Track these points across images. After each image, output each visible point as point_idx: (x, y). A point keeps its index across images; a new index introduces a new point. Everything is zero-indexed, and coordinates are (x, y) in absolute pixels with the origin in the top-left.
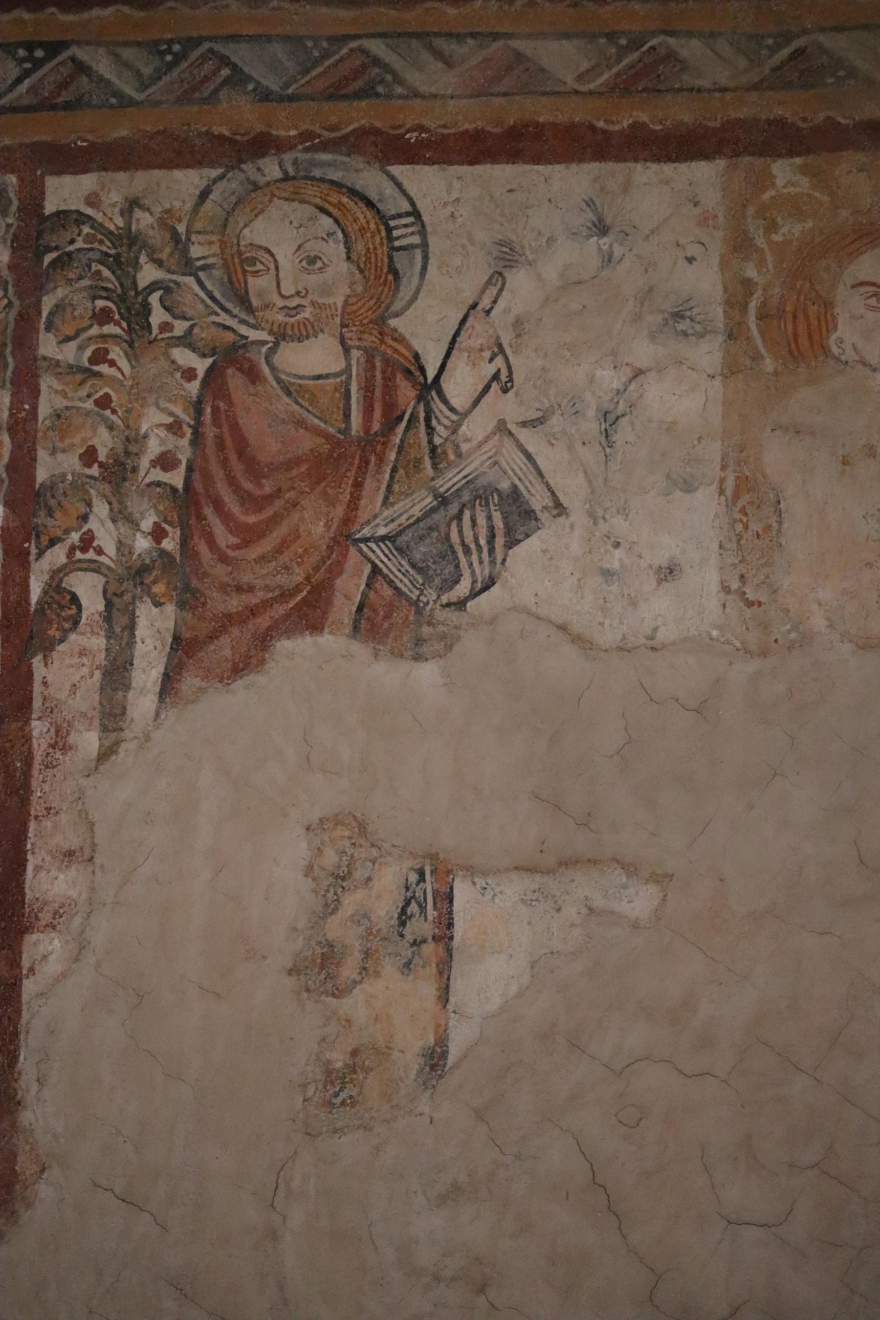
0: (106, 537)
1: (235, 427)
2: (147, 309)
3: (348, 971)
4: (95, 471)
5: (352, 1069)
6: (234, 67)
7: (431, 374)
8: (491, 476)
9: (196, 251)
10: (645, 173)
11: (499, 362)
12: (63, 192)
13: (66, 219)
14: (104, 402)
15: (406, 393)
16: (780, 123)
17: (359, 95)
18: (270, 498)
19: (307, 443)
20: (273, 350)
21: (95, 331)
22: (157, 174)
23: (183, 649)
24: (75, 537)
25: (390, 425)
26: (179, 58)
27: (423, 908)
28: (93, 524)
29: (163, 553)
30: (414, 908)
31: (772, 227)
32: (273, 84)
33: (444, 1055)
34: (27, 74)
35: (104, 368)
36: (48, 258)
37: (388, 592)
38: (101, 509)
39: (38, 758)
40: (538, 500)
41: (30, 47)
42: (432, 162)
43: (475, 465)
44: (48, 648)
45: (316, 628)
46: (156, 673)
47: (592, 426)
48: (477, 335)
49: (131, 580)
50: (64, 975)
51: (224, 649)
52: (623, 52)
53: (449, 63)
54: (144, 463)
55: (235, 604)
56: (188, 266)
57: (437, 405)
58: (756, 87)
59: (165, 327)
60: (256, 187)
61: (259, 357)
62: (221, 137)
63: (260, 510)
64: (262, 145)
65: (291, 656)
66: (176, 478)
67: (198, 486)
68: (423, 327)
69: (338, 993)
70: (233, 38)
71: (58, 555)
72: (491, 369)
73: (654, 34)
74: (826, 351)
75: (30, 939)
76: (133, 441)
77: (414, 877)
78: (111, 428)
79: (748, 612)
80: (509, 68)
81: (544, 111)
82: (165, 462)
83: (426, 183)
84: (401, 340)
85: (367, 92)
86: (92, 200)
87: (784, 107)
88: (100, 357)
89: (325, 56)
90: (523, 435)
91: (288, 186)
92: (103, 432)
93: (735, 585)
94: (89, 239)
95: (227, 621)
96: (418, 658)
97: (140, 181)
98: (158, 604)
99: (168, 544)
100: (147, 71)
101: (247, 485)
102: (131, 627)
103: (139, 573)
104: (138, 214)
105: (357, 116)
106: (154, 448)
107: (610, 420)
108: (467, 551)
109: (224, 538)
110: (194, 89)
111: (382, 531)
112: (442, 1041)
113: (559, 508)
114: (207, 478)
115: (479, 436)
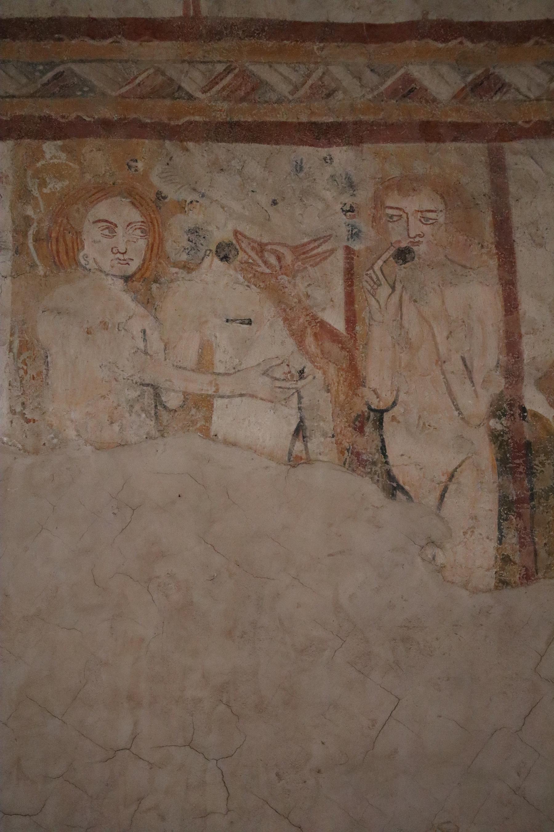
31: (43, 184)
58: (32, 96)
87: (52, 109)
93: (19, 409)
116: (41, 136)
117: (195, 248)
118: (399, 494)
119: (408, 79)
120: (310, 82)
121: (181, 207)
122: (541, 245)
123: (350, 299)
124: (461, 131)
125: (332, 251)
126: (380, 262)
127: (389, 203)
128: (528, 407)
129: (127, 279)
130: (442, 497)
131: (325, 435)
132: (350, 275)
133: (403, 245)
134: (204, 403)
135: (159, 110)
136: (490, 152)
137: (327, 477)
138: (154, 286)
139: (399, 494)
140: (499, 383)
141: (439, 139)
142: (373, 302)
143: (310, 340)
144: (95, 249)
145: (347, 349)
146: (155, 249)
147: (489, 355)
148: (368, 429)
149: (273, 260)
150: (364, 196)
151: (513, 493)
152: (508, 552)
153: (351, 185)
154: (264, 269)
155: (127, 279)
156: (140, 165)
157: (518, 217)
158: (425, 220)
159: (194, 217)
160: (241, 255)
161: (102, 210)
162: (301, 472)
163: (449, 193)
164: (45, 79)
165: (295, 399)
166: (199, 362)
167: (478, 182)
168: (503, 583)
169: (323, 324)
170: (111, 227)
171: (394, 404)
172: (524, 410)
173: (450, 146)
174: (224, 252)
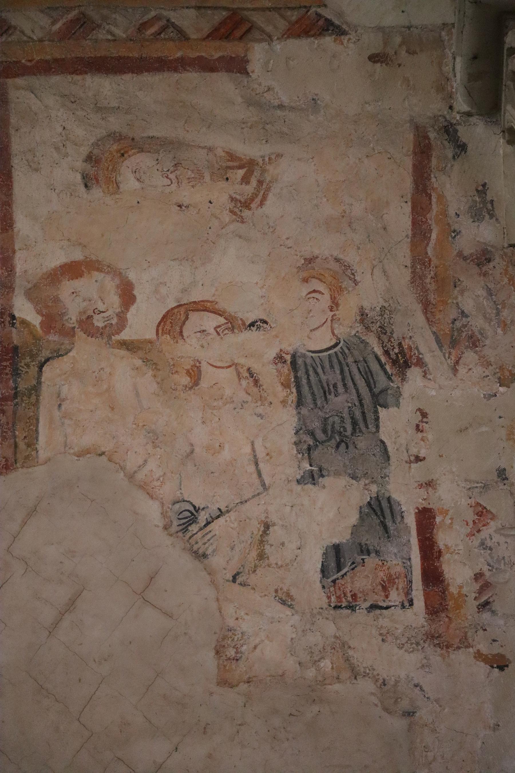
172: (13, 317)
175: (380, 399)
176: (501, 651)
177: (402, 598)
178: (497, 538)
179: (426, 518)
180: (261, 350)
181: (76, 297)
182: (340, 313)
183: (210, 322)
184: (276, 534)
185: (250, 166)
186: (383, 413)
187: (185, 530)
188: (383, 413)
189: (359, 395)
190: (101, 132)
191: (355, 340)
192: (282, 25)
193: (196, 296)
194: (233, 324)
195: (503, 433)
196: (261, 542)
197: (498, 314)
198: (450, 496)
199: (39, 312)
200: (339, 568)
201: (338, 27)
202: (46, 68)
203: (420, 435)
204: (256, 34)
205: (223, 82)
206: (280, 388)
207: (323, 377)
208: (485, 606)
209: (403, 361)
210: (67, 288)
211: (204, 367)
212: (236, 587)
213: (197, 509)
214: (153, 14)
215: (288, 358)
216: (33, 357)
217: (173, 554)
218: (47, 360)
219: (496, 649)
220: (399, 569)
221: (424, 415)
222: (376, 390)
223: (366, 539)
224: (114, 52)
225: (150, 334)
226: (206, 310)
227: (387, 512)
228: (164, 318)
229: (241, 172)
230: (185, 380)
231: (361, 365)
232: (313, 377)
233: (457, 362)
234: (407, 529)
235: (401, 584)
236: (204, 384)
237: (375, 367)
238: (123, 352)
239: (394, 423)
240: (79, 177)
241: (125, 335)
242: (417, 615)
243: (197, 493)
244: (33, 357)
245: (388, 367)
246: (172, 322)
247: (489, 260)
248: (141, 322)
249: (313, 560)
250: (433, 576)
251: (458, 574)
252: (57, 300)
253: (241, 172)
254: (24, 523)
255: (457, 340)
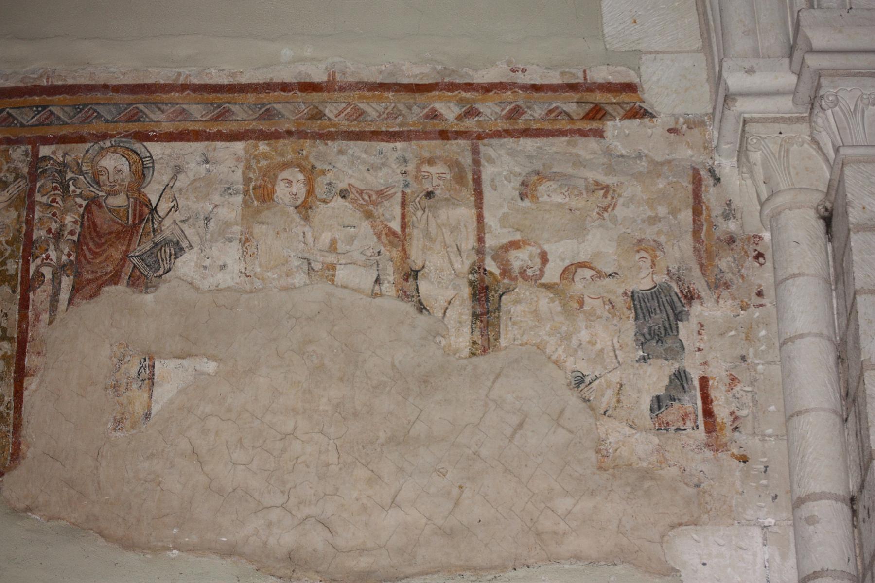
0: (53, 255)
1: (94, 222)
2: (68, 186)
3: (122, 389)
4: (51, 235)
5: (122, 419)
6: (98, 113)
7: (154, 205)
8: (171, 237)
9: (84, 168)
10: (219, 144)
11: (175, 202)
12: (45, 151)
13: (45, 158)
14: (54, 215)
15: (146, 210)
16: (261, 130)
17: (135, 121)
18: (103, 244)
19: (116, 227)
20: (106, 199)
21: (52, 193)
22: (74, 145)
23: (76, 289)
24: (44, 255)
25: (140, 222)
26: (81, 110)
27: (145, 370)
28: (50, 252)
29: (71, 261)
30: (142, 370)
31: (258, 162)
32: (109, 118)
33: (150, 414)
34: (36, 115)
35: (55, 204)
36: (40, 171)
37: (138, 273)
38: (52, 247)
39: (30, 323)
40: (184, 244)
41: (37, 107)
42: (157, 141)
43: (167, 233)
44: (34, 290)
45: (116, 284)
46: (67, 297)
47: (202, 223)
48: (168, 194)
49: (60, 269)
50: (36, 390)
51: (88, 290)
52: (215, 109)
53: (163, 112)
54: (66, 233)
55: (90, 277)
56: (81, 173)
57: (156, 216)
58: (254, 120)
59: (74, 191)
60: (102, 148)
61: (101, 200)
62: (93, 134)
63: (101, 247)
64: (105, 136)
65: (108, 292)
66: (75, 238)
67: (81, 240)
68: (152, 193)
69: (118, 396)
70: (99, 104)
71: (38, 261)
72: (172, 204)
73: (225, 103)
74: (273, 200)
75: (26, 379)
76: (63, 226)
77: (143, 360)
78: (56, 222)
79: (247, 279)
80: (181, 113)
81: (191, 127)
82: (72, 233)
83: (156, 149)
84: (145, 195)
85: (138, 120)
86: (54, 153)
87: (264, 126)
88: (54, 201)
89: (126, 109)
90: (180, 224)
91: (112, 149)
92: (54, 223)
93: (243, 271)
94: (52, 165)
95: (89, 282)
96: (147, 293)
97: (68, 147)
98: (68, 276)
99: (72, 258)
100: (72, 114)
101: (97, 240)
102: (60, 283)
103: (63, 266)
104: (67, 157)
105: (134, 127)
106: (69, 228)
107: (207, 219)
108: (163, 261)
109: (89, 256)
110: (86, 120)
111: (137, 254)
112: (149, 407)
113: (191, 247)
114: (85, 237)
115: (168, 229)
116: (258, 139)
117: (330, 192)
118: (424, 311)
119: (434, 110)
120: (387, 112)
121: (323, 172)
122: (495, 190)
123: (403, 216)
124: (459, 134)
125: (395, 193)
126: (418, 199)
127: (423, 170)
128: (487, 268)
129: (296, 208)
130: (445, 312)
131: (389, 282)
132: (404, 204)
133: (430, 189)
134: (333, 267)
135: (315, 126)
136: (473, 144)
137: (391, 301)
138: (309, 211)
139: (424, 311)
140: (474, 257)
141: (448, 139)
142: (414, 218)
143: (383, 236)
144: (282, 191)
145: (399, 239)
146: (310, 192)
147: (470, 242)
148: (411, 280)
149: (367, 198)
150: (411, 167)
151: (479, 311)
152: (476, 339)
153: (406, 161)
154: (362, 202)
155: (296, 208)
156: (304, 152)
157: (486, 176)
158: (440, 178)
159: (329, 177)
160: (352, 195)
161: (286, 174)
162: (378, 300)
163: (454, 165)
164: (261, 112)
165: (375, 265)
166: (330, 247)
167: (467, 160)
168: (473, 354)
169: (390, 229)
170: (290, 182)
171: (423, 267)
172: (485, 270)
173: (454, 142)
174: (344, 194)
175: (679, 316)
176: (745, 453)
177: (693, 424)
178: (741, 393)
179: (704, 381)
180: (617, 289)
181: (519, 259)
182: (657, 268)
183: (588, 273)
184: (626, 388)
185: (606, 188)
186: (680, 324)
187: (578, 387)
188: (680, 324)
189: (667, 315)
190: (530, 170)
191: (665, 285)
192: (622, 112)
193: (582, 258)
194: (600, 275)
195: (743, 336)
196: (618, 394)
197: (739, 271)
198: (718, 372)
199: (499, 267)
200: (659, 408)
201: (651, 114)
202: (498, 134)
203: (700, 337)
204: (608, 117)
205: (592, 143)
206: (625, 310)
207: (648, 304)
208: (736, 429)
209: (690, 297)
210: (513, 254)
211: (586, 299)
212: (605, 417)
213: (584, 376)
214: (554, 105)
215: (630, 294)
216: (496, 291)
217: (573, 400)
218: (503, 294)
219: (742, 452)
220: (691, 409)
221: (702, 326)
222: (781, 274)
223: (673, 393)
224: (534, 127)
225: (556, 280)
226: (586, 267)
227: (684, 378)
228: (564, 271)
229: (602, 192)
230: (576, 305)
231: (668, 298)
232: (643, 304)
233: (719, 298)
234: (695, 389)
235: (692, 417)
236: (586, 308)
237: (675, 299)
238: (543, 290)
239: (685, 331)
240: (517, 193)
241: (543, 281)
242: (701, 434)
243: (584, 367)
244: (496, 291)
245: (682, 299)
246: (568, 273)
247: (734, 242)
248: (552, 273)
249: (646, 402)
250: (708, 413)
251: (721, 412)
252: (508, 261)
253: (602, 192)
254: (494, 382)
255: (719, 285)
